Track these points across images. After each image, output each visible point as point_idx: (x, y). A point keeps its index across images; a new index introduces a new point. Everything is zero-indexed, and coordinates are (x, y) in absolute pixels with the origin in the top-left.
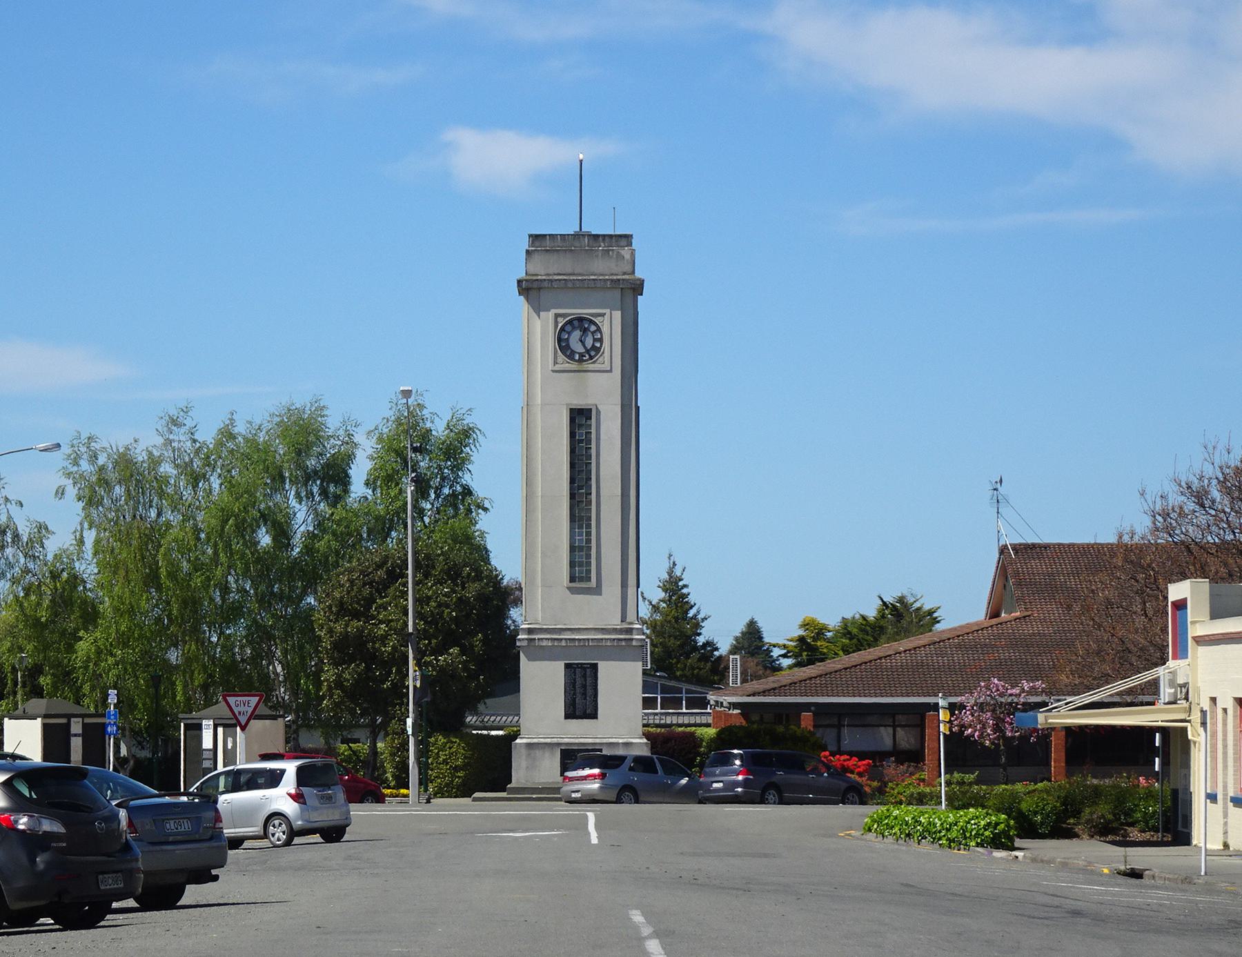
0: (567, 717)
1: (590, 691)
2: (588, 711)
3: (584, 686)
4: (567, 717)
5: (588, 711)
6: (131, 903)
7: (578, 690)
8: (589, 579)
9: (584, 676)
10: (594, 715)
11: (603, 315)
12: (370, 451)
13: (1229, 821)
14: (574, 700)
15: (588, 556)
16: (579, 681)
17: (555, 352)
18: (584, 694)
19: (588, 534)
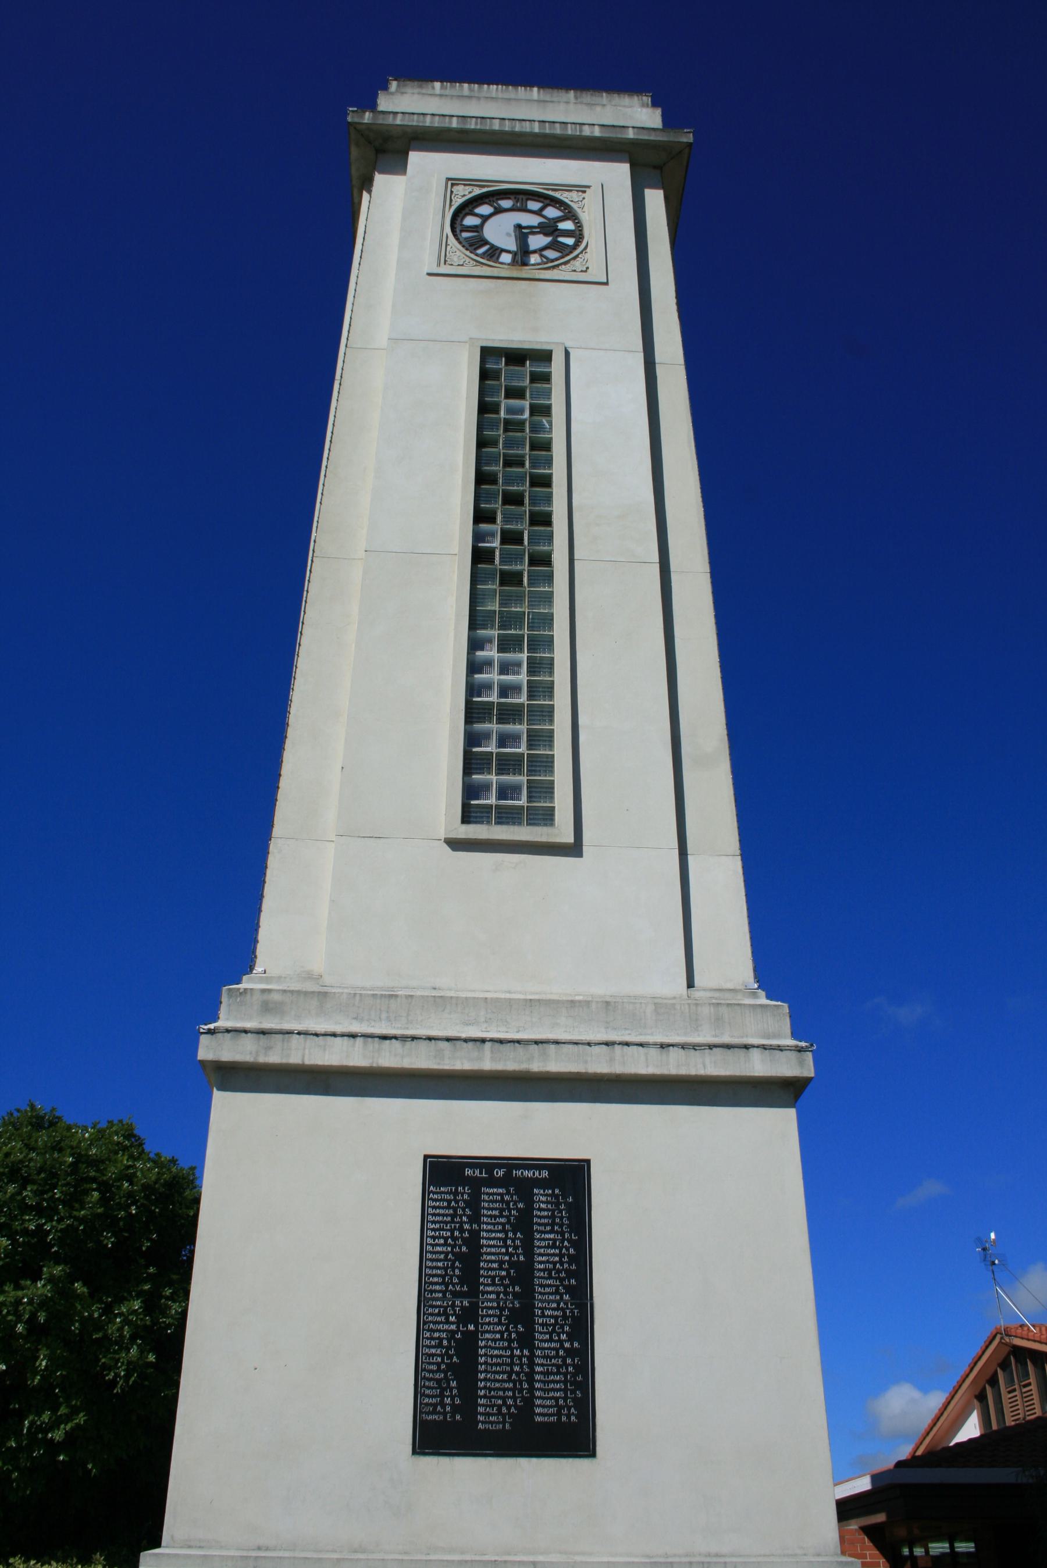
0: (441, 1432)
1: (548, 1303)
2: (543, 1412)
3: (522, 1274)
4: (441, 1432)
5: (543, 1412)
6: (468, 1172)
7: (490, 1296)
8: (547, 817)
9: (524, 1223)
10: (569, 1434)
11: (582, 189)
12: (916, 1394)
13: (338, 1039)
14: (467, 1346)
15: (542, 738)
16: (494, 1247)
17: (443, 244)
18: (523, 1315)
19: (541, 666)
